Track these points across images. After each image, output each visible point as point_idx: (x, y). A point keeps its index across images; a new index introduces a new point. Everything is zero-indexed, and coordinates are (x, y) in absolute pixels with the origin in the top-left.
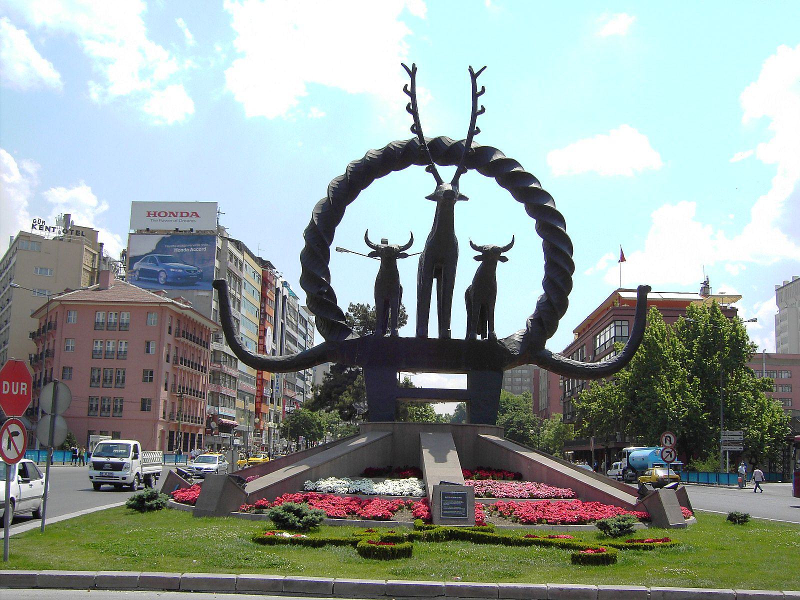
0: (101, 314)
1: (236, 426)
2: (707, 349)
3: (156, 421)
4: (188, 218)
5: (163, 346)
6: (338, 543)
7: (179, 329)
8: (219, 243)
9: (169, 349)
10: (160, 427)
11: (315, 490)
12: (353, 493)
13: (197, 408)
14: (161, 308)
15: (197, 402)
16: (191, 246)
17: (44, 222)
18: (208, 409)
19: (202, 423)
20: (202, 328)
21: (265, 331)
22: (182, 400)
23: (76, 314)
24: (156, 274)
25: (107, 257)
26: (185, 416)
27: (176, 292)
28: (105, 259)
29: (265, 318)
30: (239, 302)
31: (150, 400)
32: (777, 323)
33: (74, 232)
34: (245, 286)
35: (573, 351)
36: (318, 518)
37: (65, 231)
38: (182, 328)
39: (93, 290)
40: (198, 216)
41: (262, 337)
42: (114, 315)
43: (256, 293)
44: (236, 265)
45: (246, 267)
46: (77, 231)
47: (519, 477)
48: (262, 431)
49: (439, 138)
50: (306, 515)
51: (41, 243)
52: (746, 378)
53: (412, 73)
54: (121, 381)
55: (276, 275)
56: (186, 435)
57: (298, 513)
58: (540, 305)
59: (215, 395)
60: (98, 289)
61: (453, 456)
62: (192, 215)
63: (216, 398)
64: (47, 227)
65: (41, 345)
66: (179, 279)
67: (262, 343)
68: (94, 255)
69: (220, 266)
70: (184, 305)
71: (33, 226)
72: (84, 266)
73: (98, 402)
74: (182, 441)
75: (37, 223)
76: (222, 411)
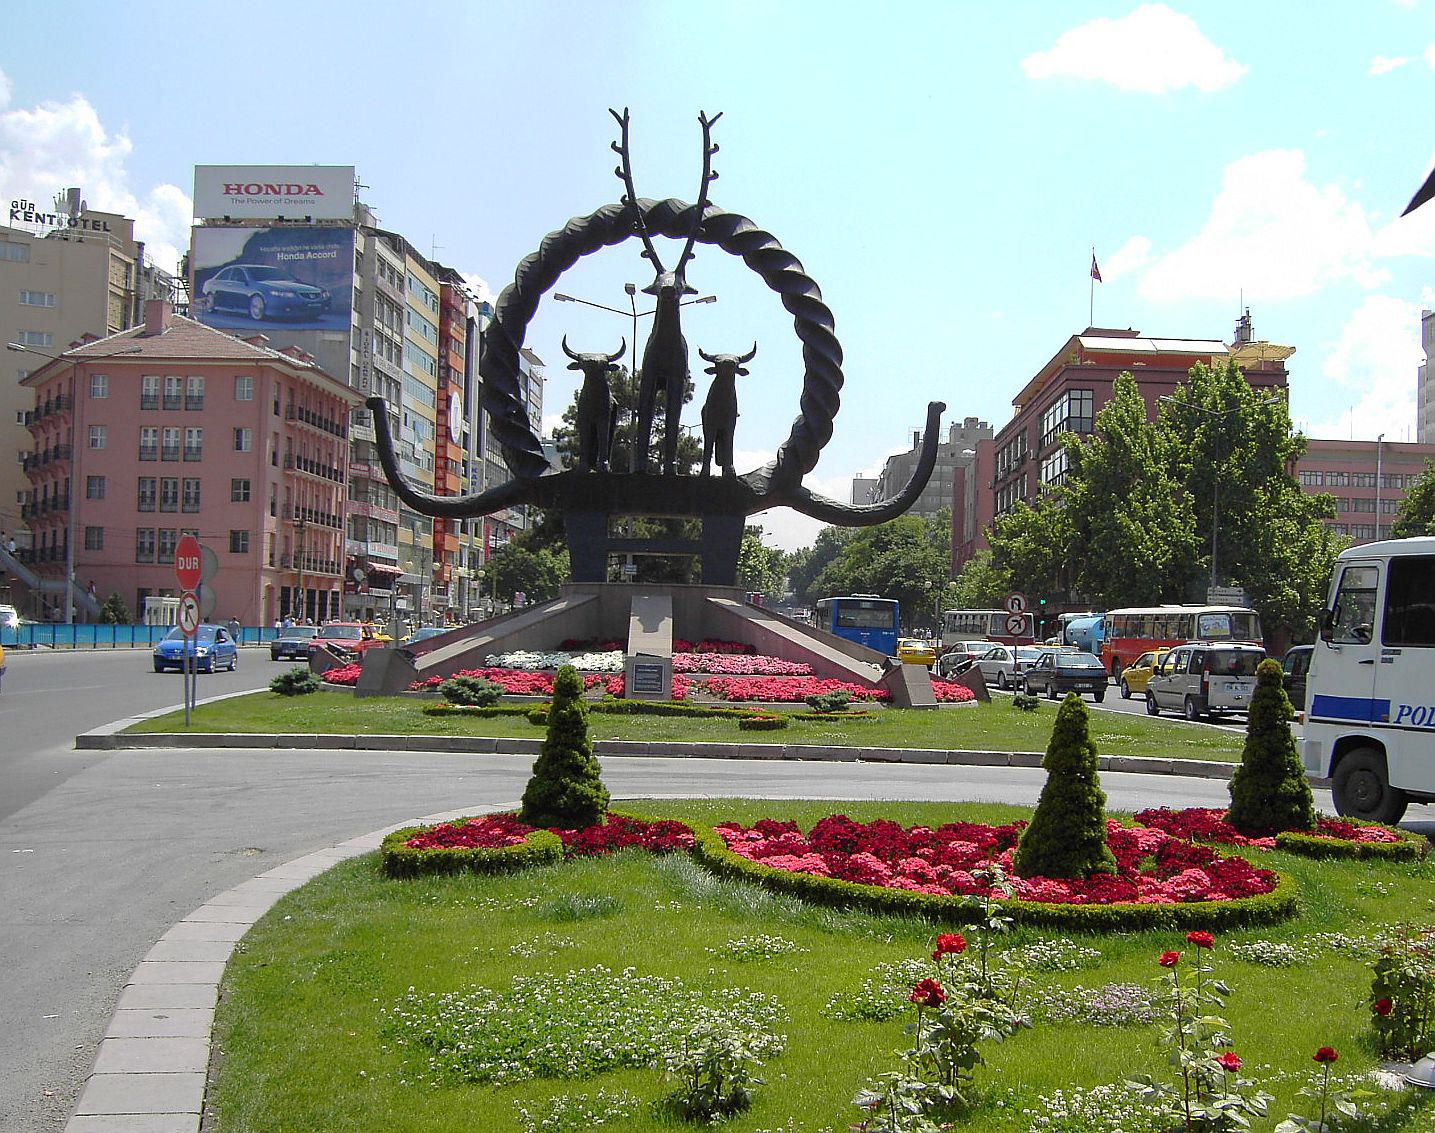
0: (152, 380)
1: (400, 575)
2: (1215, 448)
3: (258, 571)
4: (301, 197)
5: (266, 438)
6: (511, 713)
7: (292, 406)
8: (359, 242)
9: (277, 443)
10: (265, 581)
11: (499, 666)
12: (544, 669)
13: (328, 546)
14: (260, 368)
15: (329, 535)
16: (307, 248)
17: (32, 206)
18: (347, 546)
19: (339, 572)
20: (333, 401)
21: (448, 399)
22: (303, 533)
23: (105, 381)
24: (245, 302)
25: (151, 268)
26: (309, 560)
27: (285, 335)
28: (148, 273)
29: (448, 376)
30: (400, 350)
31: (245, 533)
32: (1421, 384)
33: (90, 224)
34: (409, 318)
35: (1009, 439)
36: (495, 693)
37: (73, 222)
38: (298, 403)
39: (135, 337)
40: (319, 193)
41: (443, 412)
42: (174, 381)
43: (430, 329)
44: (391, 281)
45: (410, 282)
46: (94, 222)
47: (751, 650)
48: (447, 584)
49: (666, 202)
50: (482, 689)
51: (28, 245)
52: (1287, 496)
53: (624, 123)
54: (192, 501)
55: (468, 293)
56: (311, 593)
57: (474, 687)
58: (797, 429)
59: (360, 521)
60: (143, 335)
61: (667, 625)
62: (309, 190)
63: (361, 527)
64: (37, 215)
65: (42, 437)
66: (288, 310)
67: (443, 422)
68: (128, 265)
69: (363, 283)
70: (300, 363)
71: (13, 215)
72: (110, 287)
73: (153, 538)
74: (305, 605)
75: (19, 208)
76: (373, 549)
